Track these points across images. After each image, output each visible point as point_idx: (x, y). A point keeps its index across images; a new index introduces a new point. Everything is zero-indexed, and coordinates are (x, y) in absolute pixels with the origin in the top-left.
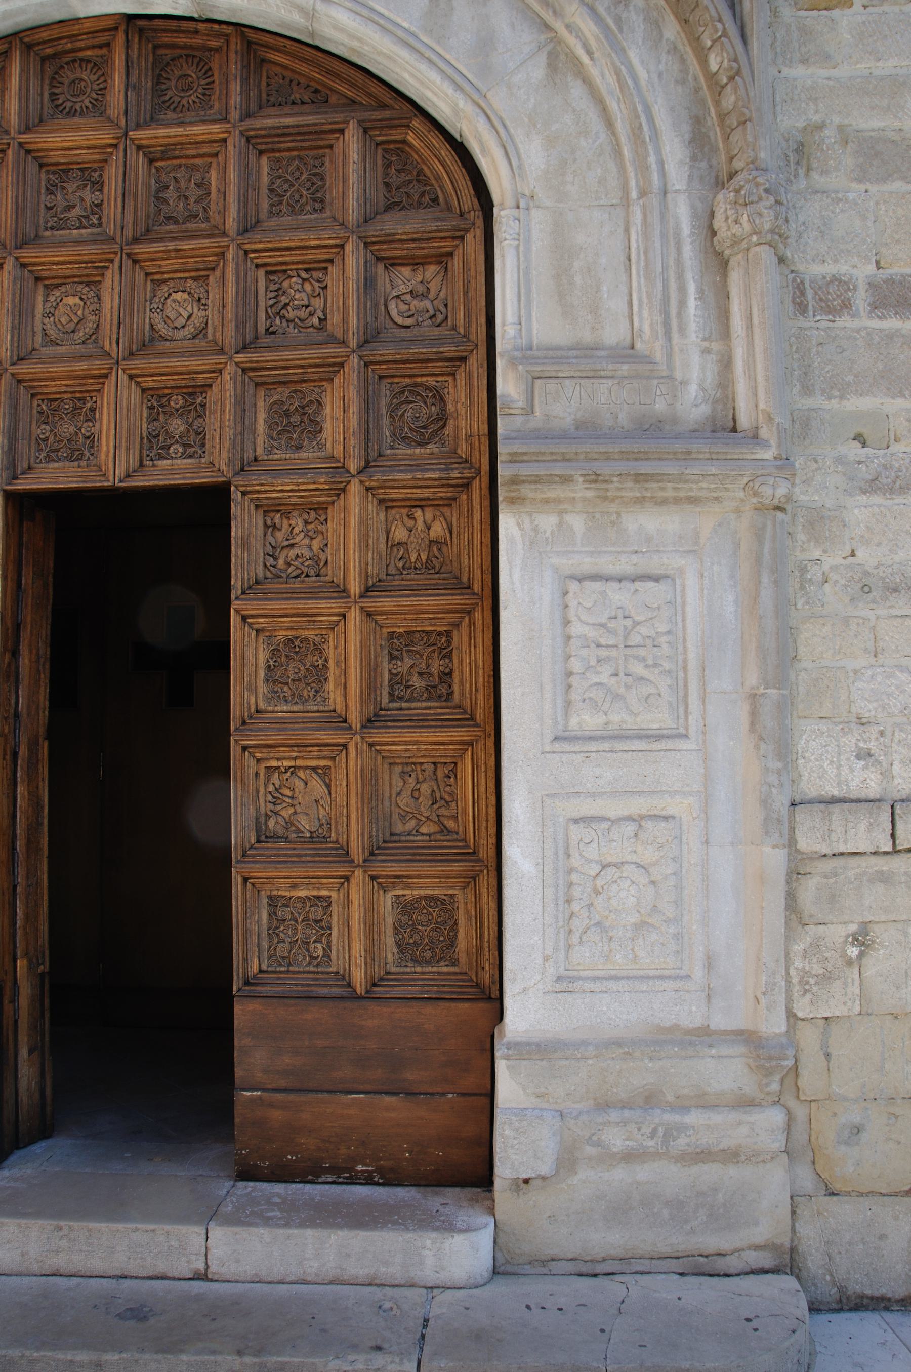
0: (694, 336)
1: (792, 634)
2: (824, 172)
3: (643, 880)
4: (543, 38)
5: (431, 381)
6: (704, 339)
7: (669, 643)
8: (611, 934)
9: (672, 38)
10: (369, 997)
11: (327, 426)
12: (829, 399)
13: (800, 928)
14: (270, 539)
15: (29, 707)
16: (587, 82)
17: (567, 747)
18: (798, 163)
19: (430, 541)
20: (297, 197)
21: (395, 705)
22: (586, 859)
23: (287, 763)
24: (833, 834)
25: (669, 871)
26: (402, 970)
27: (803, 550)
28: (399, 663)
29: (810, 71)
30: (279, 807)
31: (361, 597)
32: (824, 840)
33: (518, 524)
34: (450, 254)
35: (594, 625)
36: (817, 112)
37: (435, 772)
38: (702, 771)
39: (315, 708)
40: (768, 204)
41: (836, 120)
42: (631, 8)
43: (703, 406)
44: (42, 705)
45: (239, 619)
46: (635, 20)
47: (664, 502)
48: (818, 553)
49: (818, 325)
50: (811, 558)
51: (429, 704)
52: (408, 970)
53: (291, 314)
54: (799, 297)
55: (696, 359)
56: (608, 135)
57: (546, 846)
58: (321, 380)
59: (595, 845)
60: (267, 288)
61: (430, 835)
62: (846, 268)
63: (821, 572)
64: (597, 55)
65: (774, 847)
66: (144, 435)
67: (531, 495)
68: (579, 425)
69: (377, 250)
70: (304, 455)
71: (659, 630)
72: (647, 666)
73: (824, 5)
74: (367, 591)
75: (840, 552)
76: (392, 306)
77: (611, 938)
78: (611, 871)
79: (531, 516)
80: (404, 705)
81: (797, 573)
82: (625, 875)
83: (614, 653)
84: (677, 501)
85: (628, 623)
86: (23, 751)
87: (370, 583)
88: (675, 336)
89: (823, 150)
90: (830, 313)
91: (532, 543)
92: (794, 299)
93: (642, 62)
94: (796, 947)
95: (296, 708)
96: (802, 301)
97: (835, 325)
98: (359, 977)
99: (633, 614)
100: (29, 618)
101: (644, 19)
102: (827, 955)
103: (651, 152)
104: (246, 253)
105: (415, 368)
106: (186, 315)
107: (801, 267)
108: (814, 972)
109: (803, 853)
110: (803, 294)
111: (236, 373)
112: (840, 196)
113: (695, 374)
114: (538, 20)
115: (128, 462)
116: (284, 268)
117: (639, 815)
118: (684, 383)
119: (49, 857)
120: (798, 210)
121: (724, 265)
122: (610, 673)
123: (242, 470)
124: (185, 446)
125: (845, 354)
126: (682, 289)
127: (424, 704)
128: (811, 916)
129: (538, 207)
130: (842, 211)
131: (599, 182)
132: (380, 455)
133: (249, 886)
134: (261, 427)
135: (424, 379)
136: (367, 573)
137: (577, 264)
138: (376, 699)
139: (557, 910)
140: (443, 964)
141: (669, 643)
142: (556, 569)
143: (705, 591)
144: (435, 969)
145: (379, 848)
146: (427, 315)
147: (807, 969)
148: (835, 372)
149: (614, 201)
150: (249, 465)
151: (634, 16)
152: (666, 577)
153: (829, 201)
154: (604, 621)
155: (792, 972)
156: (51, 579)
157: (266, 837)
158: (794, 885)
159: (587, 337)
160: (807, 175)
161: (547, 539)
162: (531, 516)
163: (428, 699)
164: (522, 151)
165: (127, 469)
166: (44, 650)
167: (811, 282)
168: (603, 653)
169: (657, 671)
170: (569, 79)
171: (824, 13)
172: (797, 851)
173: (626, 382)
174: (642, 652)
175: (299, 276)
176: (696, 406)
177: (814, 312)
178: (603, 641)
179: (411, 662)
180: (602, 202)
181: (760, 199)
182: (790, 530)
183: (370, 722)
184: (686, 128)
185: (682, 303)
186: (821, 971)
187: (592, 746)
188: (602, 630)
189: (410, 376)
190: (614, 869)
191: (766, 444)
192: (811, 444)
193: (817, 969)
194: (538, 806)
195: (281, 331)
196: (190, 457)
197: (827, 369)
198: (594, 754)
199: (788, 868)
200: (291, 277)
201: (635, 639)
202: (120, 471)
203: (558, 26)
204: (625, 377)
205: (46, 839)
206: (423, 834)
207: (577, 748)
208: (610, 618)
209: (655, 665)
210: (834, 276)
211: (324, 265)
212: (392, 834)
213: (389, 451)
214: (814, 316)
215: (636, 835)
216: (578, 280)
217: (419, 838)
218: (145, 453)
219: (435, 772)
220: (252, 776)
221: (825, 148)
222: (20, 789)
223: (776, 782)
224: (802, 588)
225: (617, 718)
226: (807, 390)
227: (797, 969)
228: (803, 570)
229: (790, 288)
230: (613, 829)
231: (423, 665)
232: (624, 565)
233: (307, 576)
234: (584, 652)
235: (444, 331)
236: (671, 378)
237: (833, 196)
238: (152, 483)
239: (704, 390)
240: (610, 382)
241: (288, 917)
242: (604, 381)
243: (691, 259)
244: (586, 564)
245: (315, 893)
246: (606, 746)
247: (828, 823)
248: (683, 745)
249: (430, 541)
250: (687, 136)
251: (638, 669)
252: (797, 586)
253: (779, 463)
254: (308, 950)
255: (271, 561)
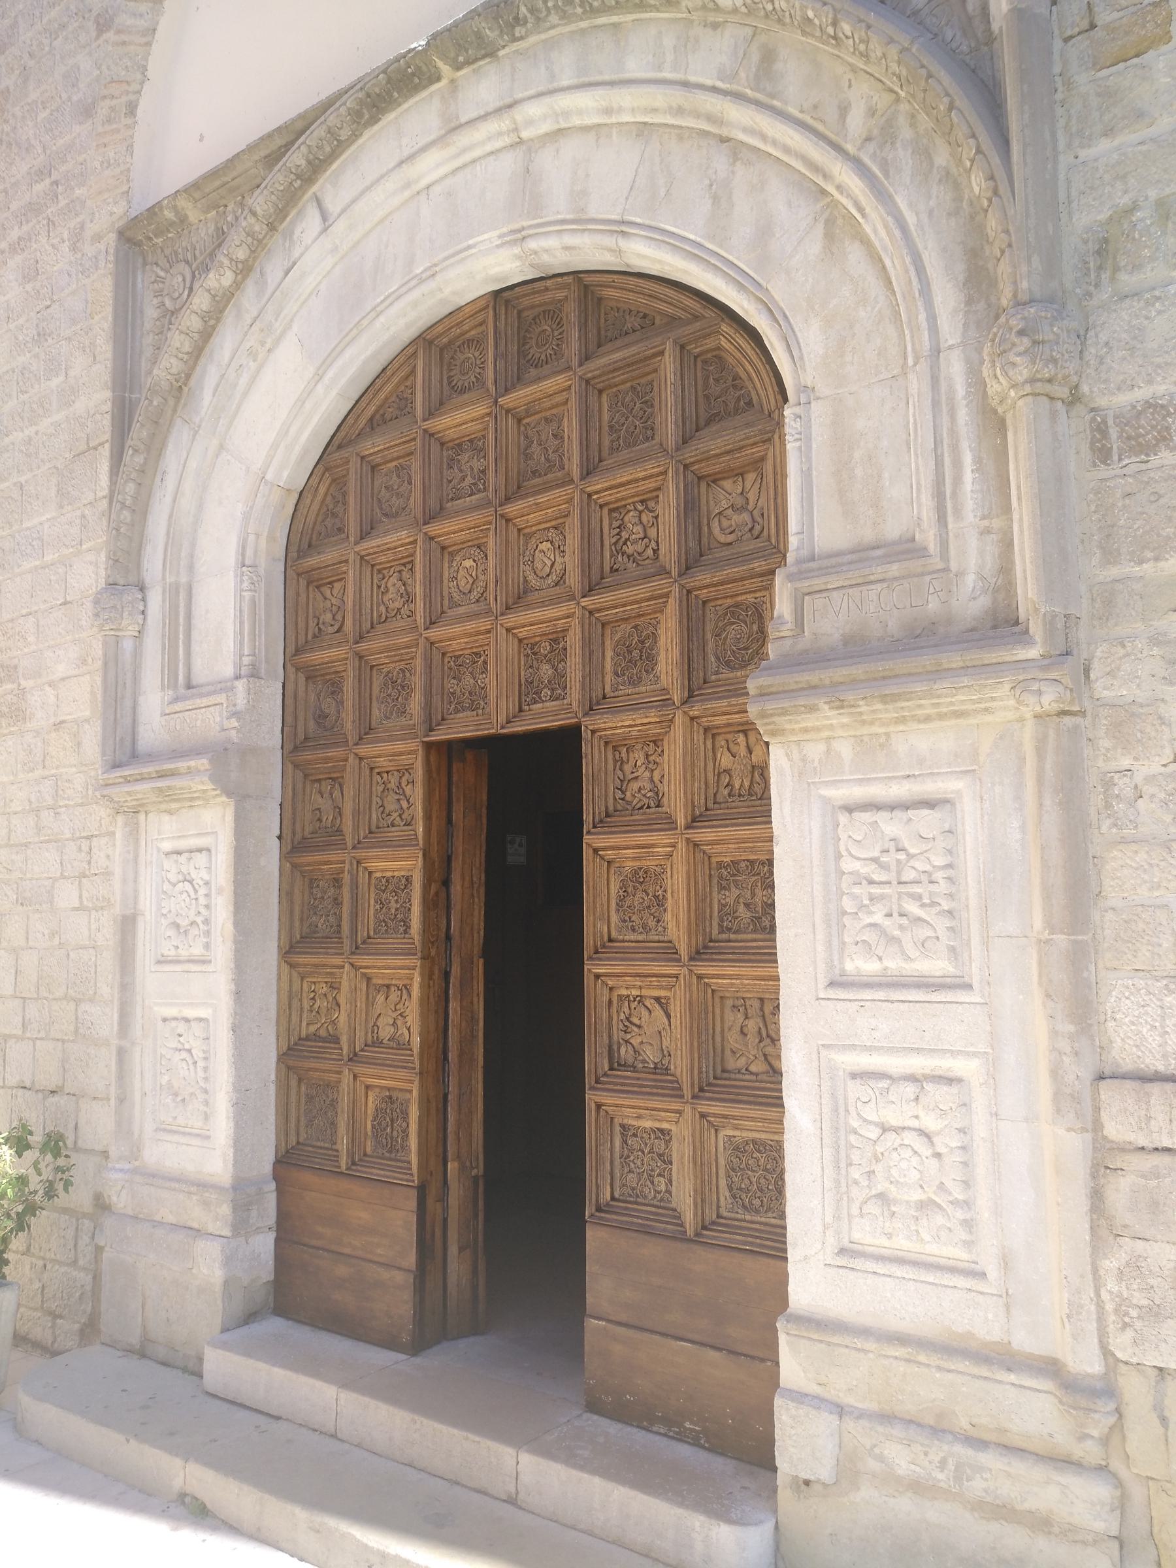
0: (971, 515)
1: (1095, 865)
2: (1136, 268)
3: (926, 1151)
4: (819, 206)
5: (750, 598)
6: (983, 518)
7: (949, 878)
8: (893, 1209)
9: (944, 164)
10: (697, 1240)
11: (662, 657)
12: (1141, 562)
13: (1111, 1238)
14: (619, 773)
15: (461, 928)
16: (866, 242)
17: (842, 994)
18: (1100, 268)
19: (753, 767)
20: (632, 429)
21: (724, 936)
22: (865, 1120)
23: (635, 992)
24: (1153, 1122)
25: (954, 1144)
26: (733, 1215)
27: (1107, 759)
28: (727, 893)
29: (1116, 142)
30: (629, 1036)
31: (688, 827)
32: (1141, 1129)
33: (787, 755)
34: (763, 459)
35: (865, 859)
36: (1126, 192)
37: (762, 1009)
38: (988, 1028)
39: (657, 938)
40: (1022, 349)
41: (1153, 194)
42: (898, 145)
43: (982, 598)
44: (476, 927)
45: (591, 851)
46: (903, 156)
47: (928, 719)
48: (1127, 762)
49: (1125, 471)
50: (1118, 769)
51: (754, 936)
52: (739, 1216)
53: (630, 549)
54: (1099, 441)
55: (973, 542)
56: (887, 296)
57: (824, 1102)
58: (656, 612)
59: (872, 1105)
60: (611, 525)
61: (757, 1075)
62: (1164, 387)
63: (1132, 786)
64: (868, 210)
65: (1069, 1130)
66: (523, 681)
67: (788, 726)
68: (847, 640)
69: (699, 469)
70: (643, 689)
71: (936, 863)
72: (923, 905)
73: (1133, 53)
74: (694, 821)
75: (1157, 758)
76: (715, 525)
77: (894, 1213)
78: (891, 1136)
79: (799, 745)
80: (732, 936)
81: (1100, 789)
82: (906, 1142)
83: (887, 890)
84: (941, 717)
85: (902, 856)
86: (455, 970)
87: (698, 813)
88: (950, 519)
89: (1134, 239)
90: (1141, 452)
91: (800, 774)
92: (1092, 444)
93: (910, 205)
94: (1108, 1262)
95: (640, 938)
96: (1103, 445)
97: (1149, 466)
98: (689, 1217)
99: (907, 846)
100: (460, 849)
101: (913, 152)
102: (1152, 1281)
103: (921, 309)
104: (590, 495)
105: (733, 587)
106: (549, 563)
107: (1102, 402)
108: (1135, 1301)
109: (1112, 1142)
110: (1104, 433)
111: (583, 615)
112: (1157, 293)
113: (972, 562)
114: (814, 188)
115: (507, 708)
116: (623, 503)
117: (923, 1075)
118: (960, 574)
119: (485, 1067)
120: (1099, 329)
121: (1001, 426)
122: (884, 913)
123: (591, 709)
124: (553, 690)
125: (1162, 501)
126: (957, 464)
127: (750, 936)
128: (1125, 1226)
129: (818, 398)
130: (1159, 312)
131: (879, 354)
132: (705, 682)
133: (602, 1113)
134: (609, 666)
135: (744, 597)
136: (693, 803)
137: (858, 454)
138: (704, 930)
139: (839, 1174)
140: (770, 1215)
141: (949, 878)
142: (826, 801)
143: (986, 817)
144: (763, 1219)
145: (709, 1084)
146: (747, 529)
147: (1125, 1295)
148: (1148, 528)
149: (895, 372)
150: (598, 703)
151: (901, 152)
152: (946, 801)
153: (1142, 303)
154: (876, 854)
155: (1105, 1296)
156: (484, 811)
157: (619, 1065)
158: (1102, 1181)
159: (868, 535)
160: (1113, 279)
161: (815, 768)
162: (799, 745)
163: (755, 931)
164: (801, 341)
165: (507, 716)
166: (479, 876)
167: (1116, 417)
168: (876, 890)
169: (934, 910)
170: (847, 243)
171: (1135, 61)
172: (1105, 1138)
173: (896, 584)
174: (917, 889)
175: (636, 509)
176: (974, 599)
177: (1120, 456)
178: (876, 877)
179: (738, 892)
180: (882, 377)
181: (1014, 345)
182: (1090, 736)
183: (698, 955)
184: (960, 268)
185: (958, 480)
186: (1145, 1302)
187: (867, 994)
188: (874, 866)
189: (731, 596)
190: (894, 1135)
191: (1031, 643)
192: (1116, 625)
193: (1140, 1299)
194: (815, 1056)
195: (622, 568)
196: (557, 699)
197: (1136, 526)
198: (868, 1003)
199: (1094, 1158)
200: (629, 511)
201: (910, 875)
202: (502, 718)
203: (830, 189)
204: (896, 579)
205: (481, 1050)
206: (752, 1073)
207: (851, 996)
208: (883, 851)
209: (934, 904)
210: (1147, 402)
211: (655, 494)
212: (724, 1071)
213: (713, 677)
214: (1120, 460)
215: (917, 1099)
216: (859, 472)
217: (747, 1077)
218: (523, 698)
219: (762, 1009)
220: (605, 1004)
221: (1137, 236)
222: (454, 1005)
223: (1068, 1050)
224: (1108, 806)
225: (894, 964)
226: (1110, 556)
227: (1111, 1292)
228: (1108, 784)
229: (1088, 432)
230: (892, 1088)
231: (749, 895)
232: (899, 791)
233: (649, 807)
234: (857, 890)
235: (759, 544)
236: (946, 570)
237: (1148, 296)
238: (523, 728)
239: (983, 578)
240: (879, 587)
241: (636, 1147)
242: (873, 587)
243: (966, 424)
244: (858, 793)
245: (657, 1125)
246: (881, 995)
247: (1144, 1106)
248: (962, 996)
249: (753, 767)
250: (961, 278)
251: (913, 908)
252: (1101, 804)
253: (1046, 662)
254: (652, 1183)
255: (619, 794)
